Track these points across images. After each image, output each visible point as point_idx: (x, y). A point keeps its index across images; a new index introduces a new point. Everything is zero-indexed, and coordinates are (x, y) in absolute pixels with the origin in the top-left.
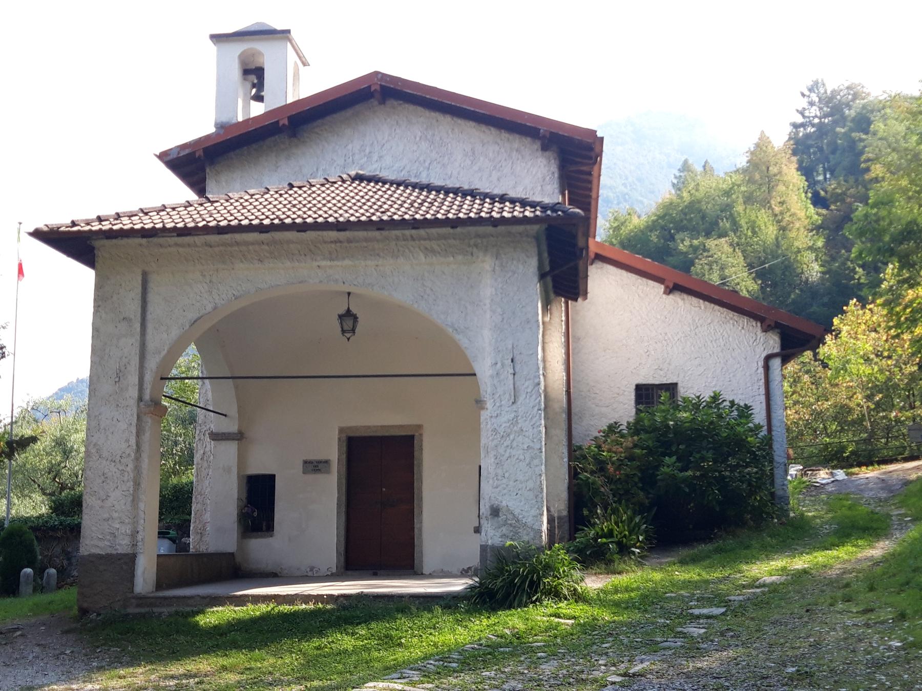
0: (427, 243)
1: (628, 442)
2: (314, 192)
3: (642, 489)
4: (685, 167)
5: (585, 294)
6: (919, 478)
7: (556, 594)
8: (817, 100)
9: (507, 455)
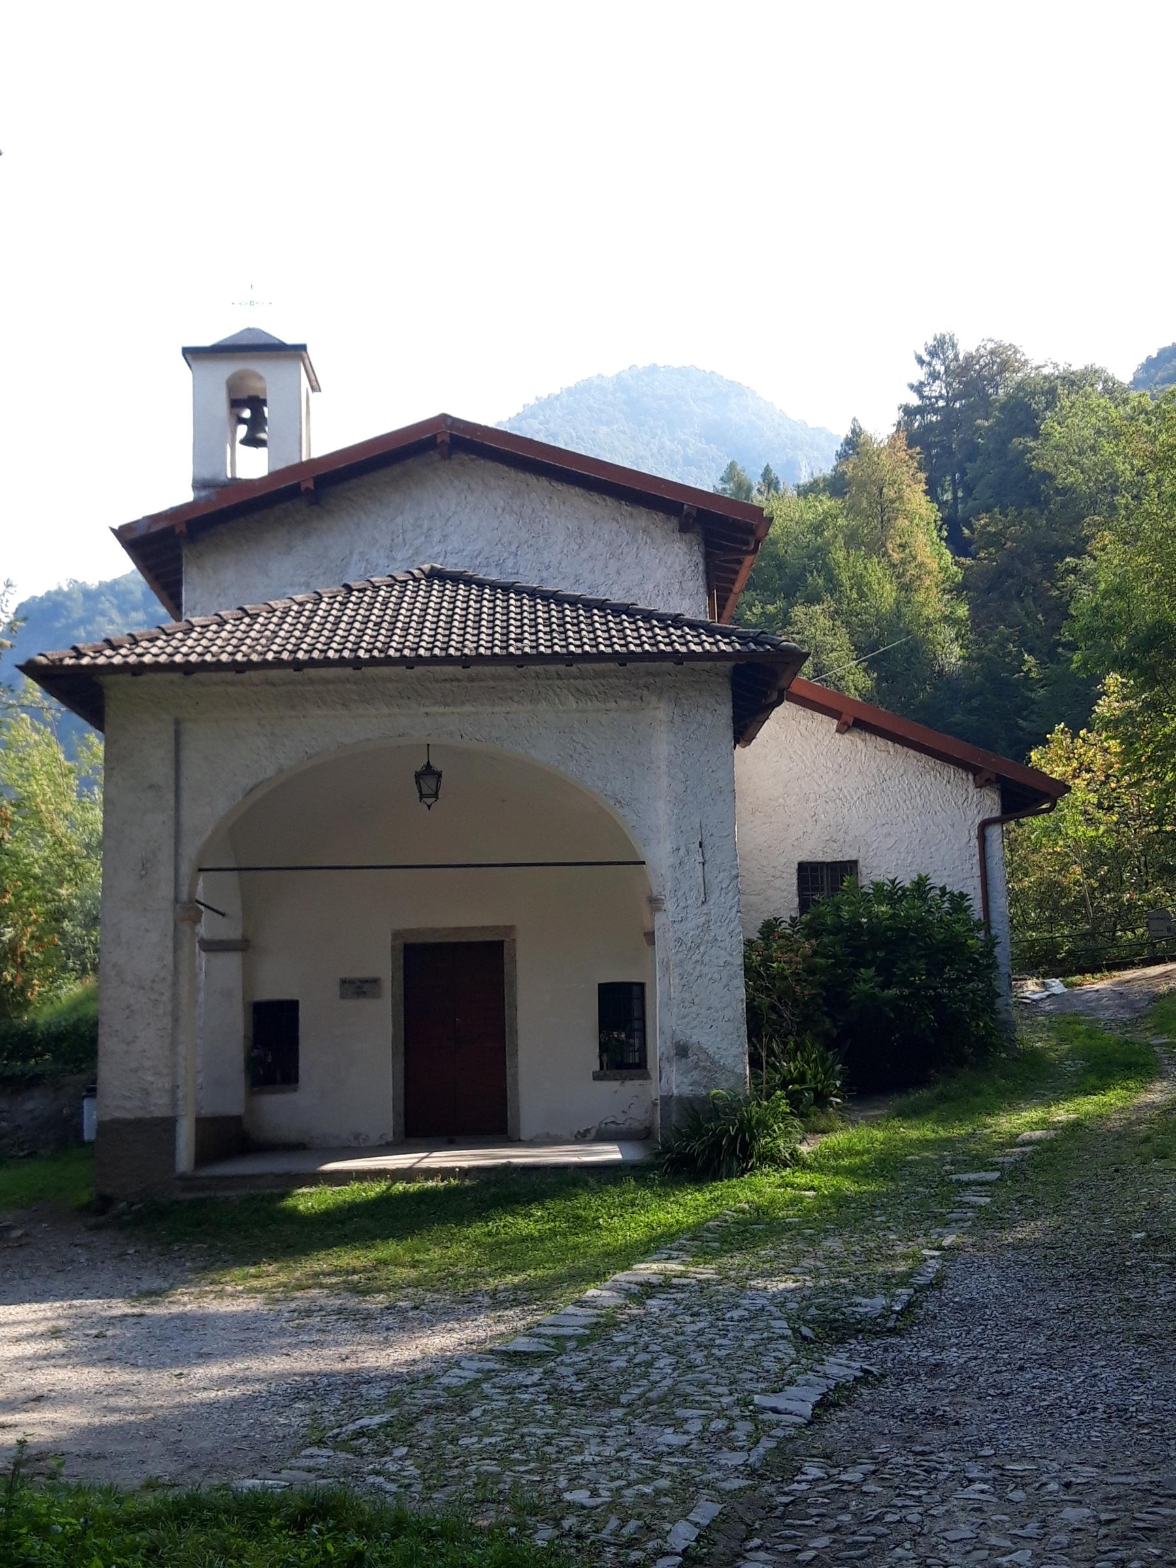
6: (1172, 992)
7: (773, 1159)
8: (942, 369)
9: (696, 974)
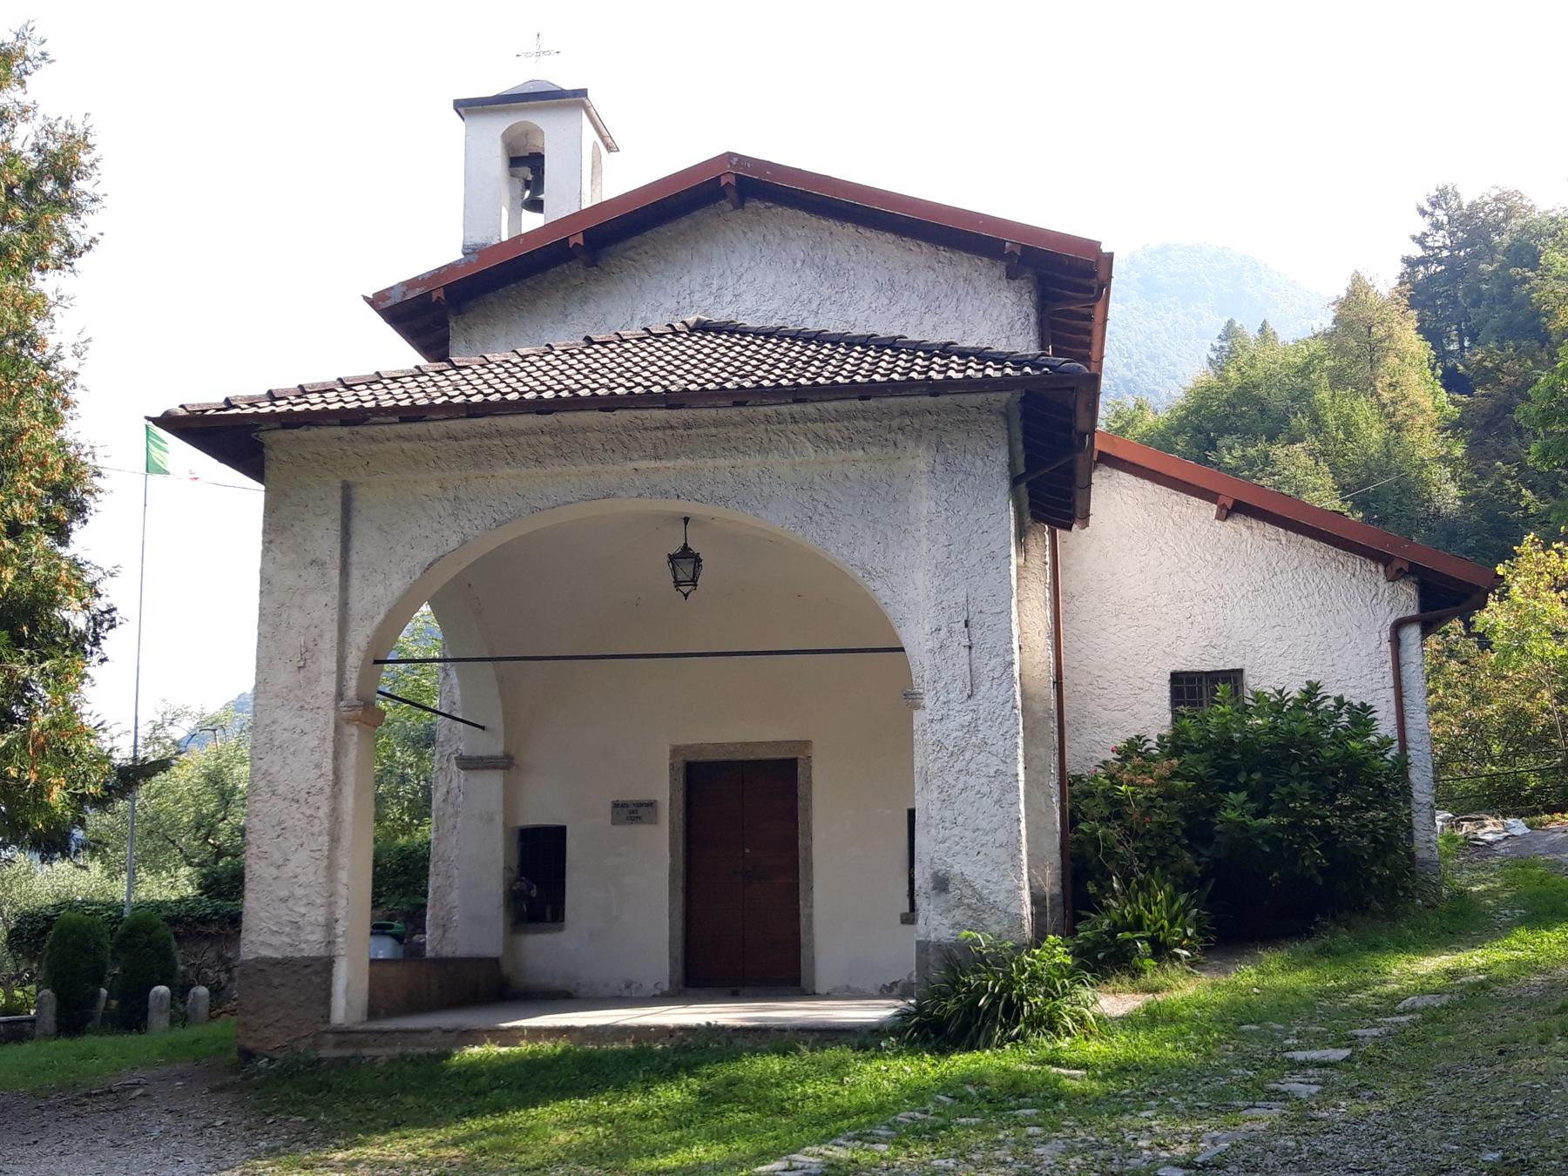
0: (818, 427)
1: (1164, 768)
2: (627, 350)
3: (1188, 848)
4: (1230, 332)
5: (1086, 517)
8: (1445, 219)
9: (960, 785)
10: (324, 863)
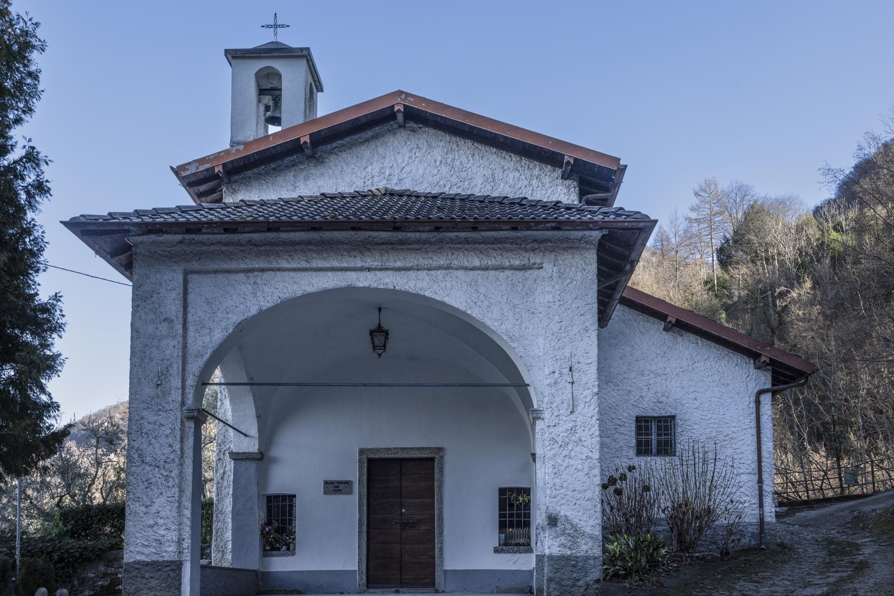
9: (565, 464)
10: (177, 504)
